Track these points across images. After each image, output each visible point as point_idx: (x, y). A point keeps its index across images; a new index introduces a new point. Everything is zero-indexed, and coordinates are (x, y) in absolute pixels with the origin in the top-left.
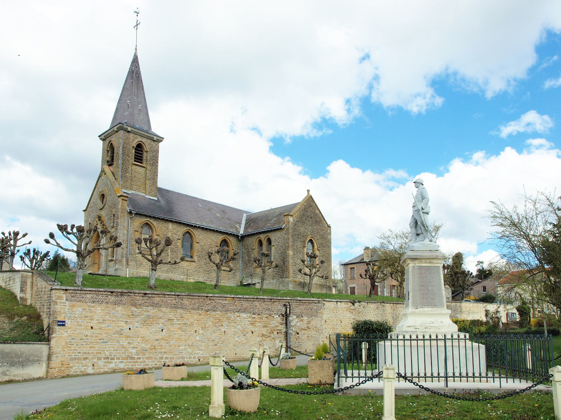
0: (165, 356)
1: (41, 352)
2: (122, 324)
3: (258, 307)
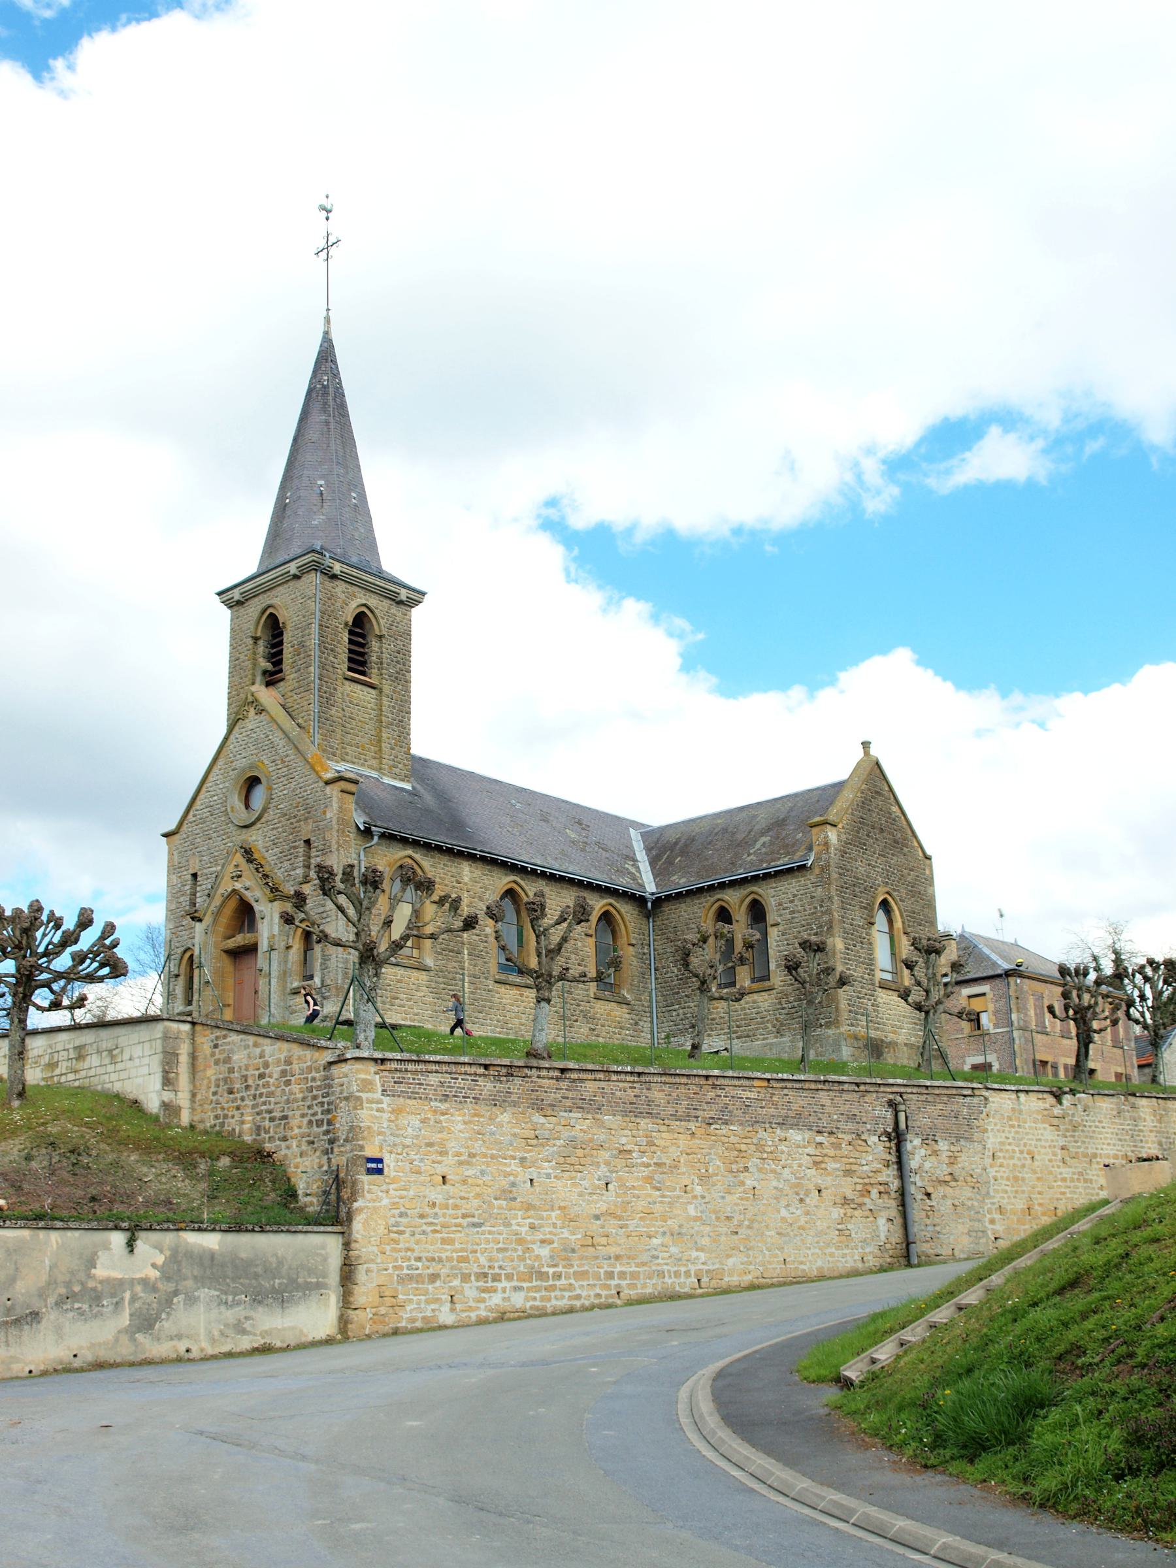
0: (618, 1268)
1: (325, 1259)
2: (514, 1166)
3: (827, 1110)
